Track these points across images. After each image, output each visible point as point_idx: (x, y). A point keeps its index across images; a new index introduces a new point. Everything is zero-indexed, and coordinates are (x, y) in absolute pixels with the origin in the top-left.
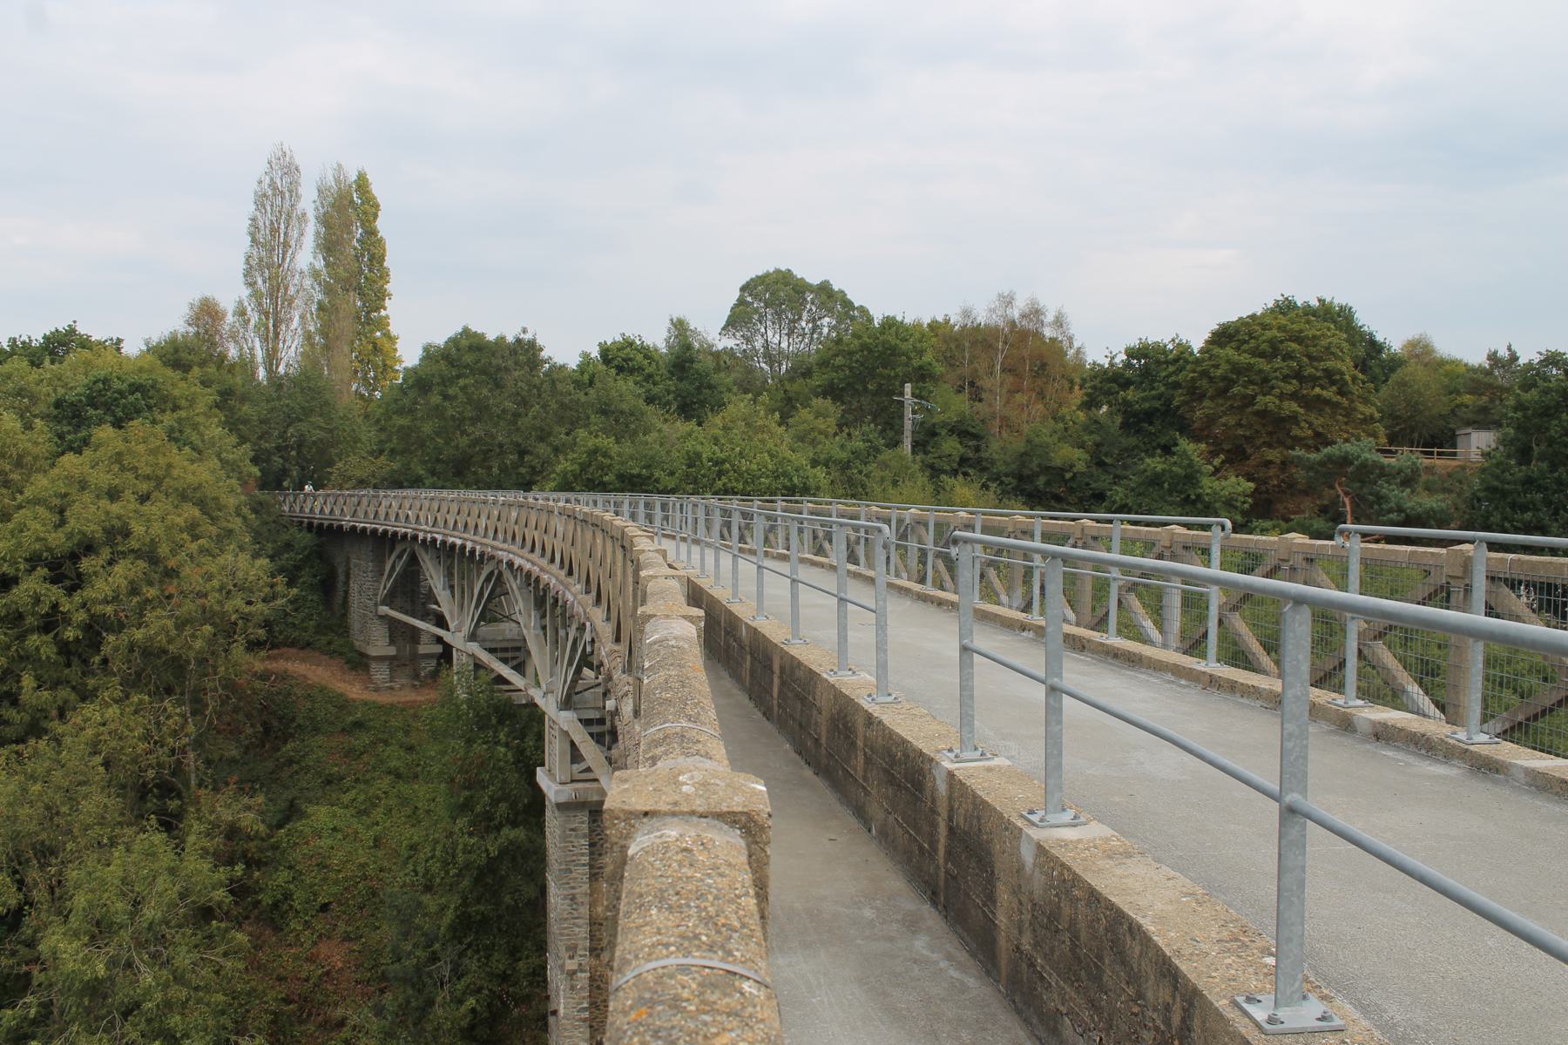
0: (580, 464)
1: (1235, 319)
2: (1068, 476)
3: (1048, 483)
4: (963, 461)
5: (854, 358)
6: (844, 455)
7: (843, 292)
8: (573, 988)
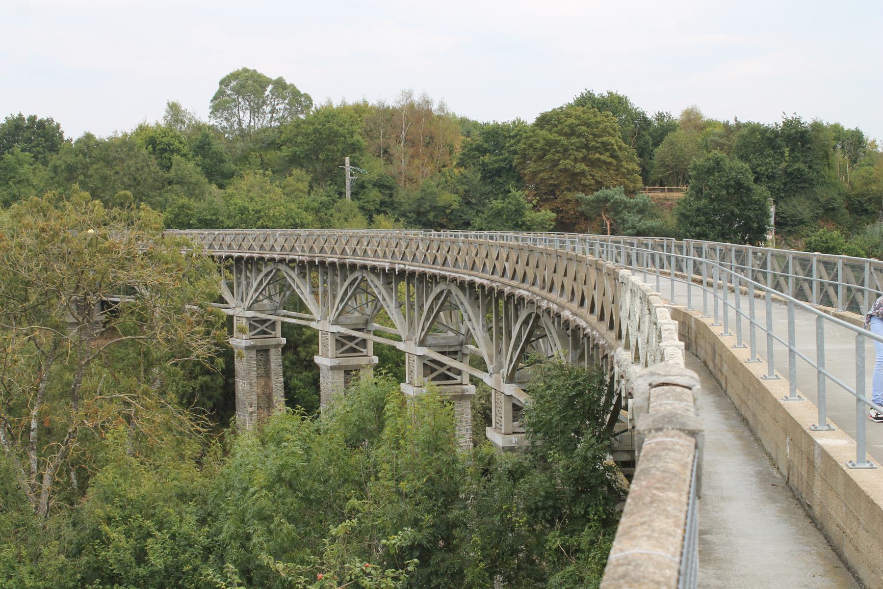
0: (174, 214)
1: (550, 110)
2: (448, 211)
3: (436, 216)
4: (382, 203)
5: (310, 138)
6: (316, 205)
7: (293, 85)
8: (251, 420)
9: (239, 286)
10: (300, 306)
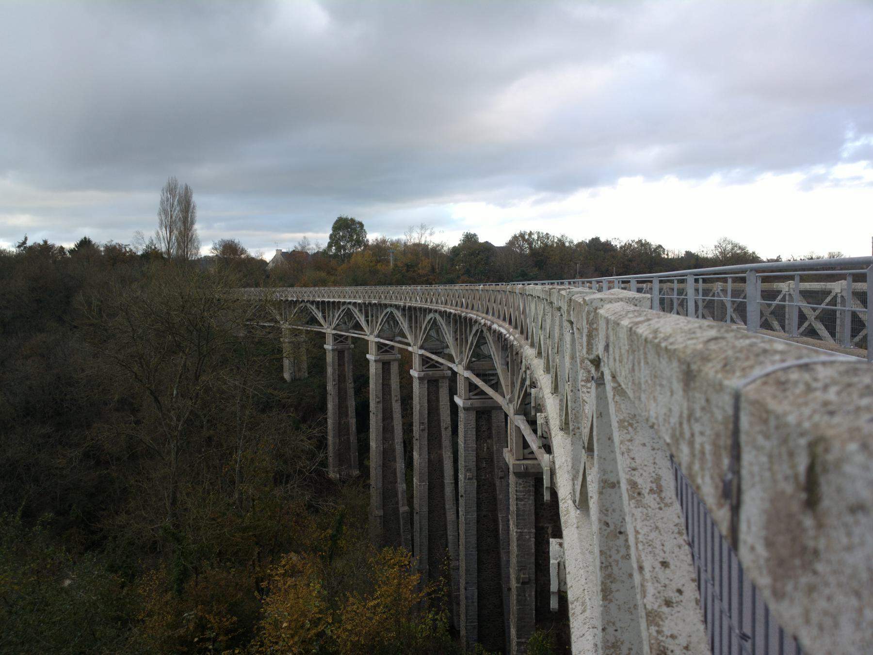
9: (328, 317)
10: (358, 327)
